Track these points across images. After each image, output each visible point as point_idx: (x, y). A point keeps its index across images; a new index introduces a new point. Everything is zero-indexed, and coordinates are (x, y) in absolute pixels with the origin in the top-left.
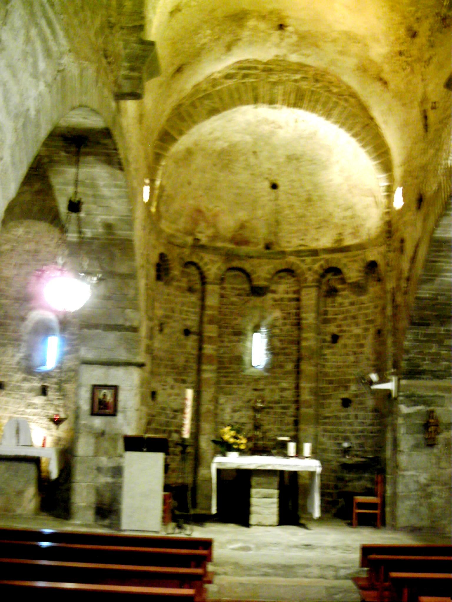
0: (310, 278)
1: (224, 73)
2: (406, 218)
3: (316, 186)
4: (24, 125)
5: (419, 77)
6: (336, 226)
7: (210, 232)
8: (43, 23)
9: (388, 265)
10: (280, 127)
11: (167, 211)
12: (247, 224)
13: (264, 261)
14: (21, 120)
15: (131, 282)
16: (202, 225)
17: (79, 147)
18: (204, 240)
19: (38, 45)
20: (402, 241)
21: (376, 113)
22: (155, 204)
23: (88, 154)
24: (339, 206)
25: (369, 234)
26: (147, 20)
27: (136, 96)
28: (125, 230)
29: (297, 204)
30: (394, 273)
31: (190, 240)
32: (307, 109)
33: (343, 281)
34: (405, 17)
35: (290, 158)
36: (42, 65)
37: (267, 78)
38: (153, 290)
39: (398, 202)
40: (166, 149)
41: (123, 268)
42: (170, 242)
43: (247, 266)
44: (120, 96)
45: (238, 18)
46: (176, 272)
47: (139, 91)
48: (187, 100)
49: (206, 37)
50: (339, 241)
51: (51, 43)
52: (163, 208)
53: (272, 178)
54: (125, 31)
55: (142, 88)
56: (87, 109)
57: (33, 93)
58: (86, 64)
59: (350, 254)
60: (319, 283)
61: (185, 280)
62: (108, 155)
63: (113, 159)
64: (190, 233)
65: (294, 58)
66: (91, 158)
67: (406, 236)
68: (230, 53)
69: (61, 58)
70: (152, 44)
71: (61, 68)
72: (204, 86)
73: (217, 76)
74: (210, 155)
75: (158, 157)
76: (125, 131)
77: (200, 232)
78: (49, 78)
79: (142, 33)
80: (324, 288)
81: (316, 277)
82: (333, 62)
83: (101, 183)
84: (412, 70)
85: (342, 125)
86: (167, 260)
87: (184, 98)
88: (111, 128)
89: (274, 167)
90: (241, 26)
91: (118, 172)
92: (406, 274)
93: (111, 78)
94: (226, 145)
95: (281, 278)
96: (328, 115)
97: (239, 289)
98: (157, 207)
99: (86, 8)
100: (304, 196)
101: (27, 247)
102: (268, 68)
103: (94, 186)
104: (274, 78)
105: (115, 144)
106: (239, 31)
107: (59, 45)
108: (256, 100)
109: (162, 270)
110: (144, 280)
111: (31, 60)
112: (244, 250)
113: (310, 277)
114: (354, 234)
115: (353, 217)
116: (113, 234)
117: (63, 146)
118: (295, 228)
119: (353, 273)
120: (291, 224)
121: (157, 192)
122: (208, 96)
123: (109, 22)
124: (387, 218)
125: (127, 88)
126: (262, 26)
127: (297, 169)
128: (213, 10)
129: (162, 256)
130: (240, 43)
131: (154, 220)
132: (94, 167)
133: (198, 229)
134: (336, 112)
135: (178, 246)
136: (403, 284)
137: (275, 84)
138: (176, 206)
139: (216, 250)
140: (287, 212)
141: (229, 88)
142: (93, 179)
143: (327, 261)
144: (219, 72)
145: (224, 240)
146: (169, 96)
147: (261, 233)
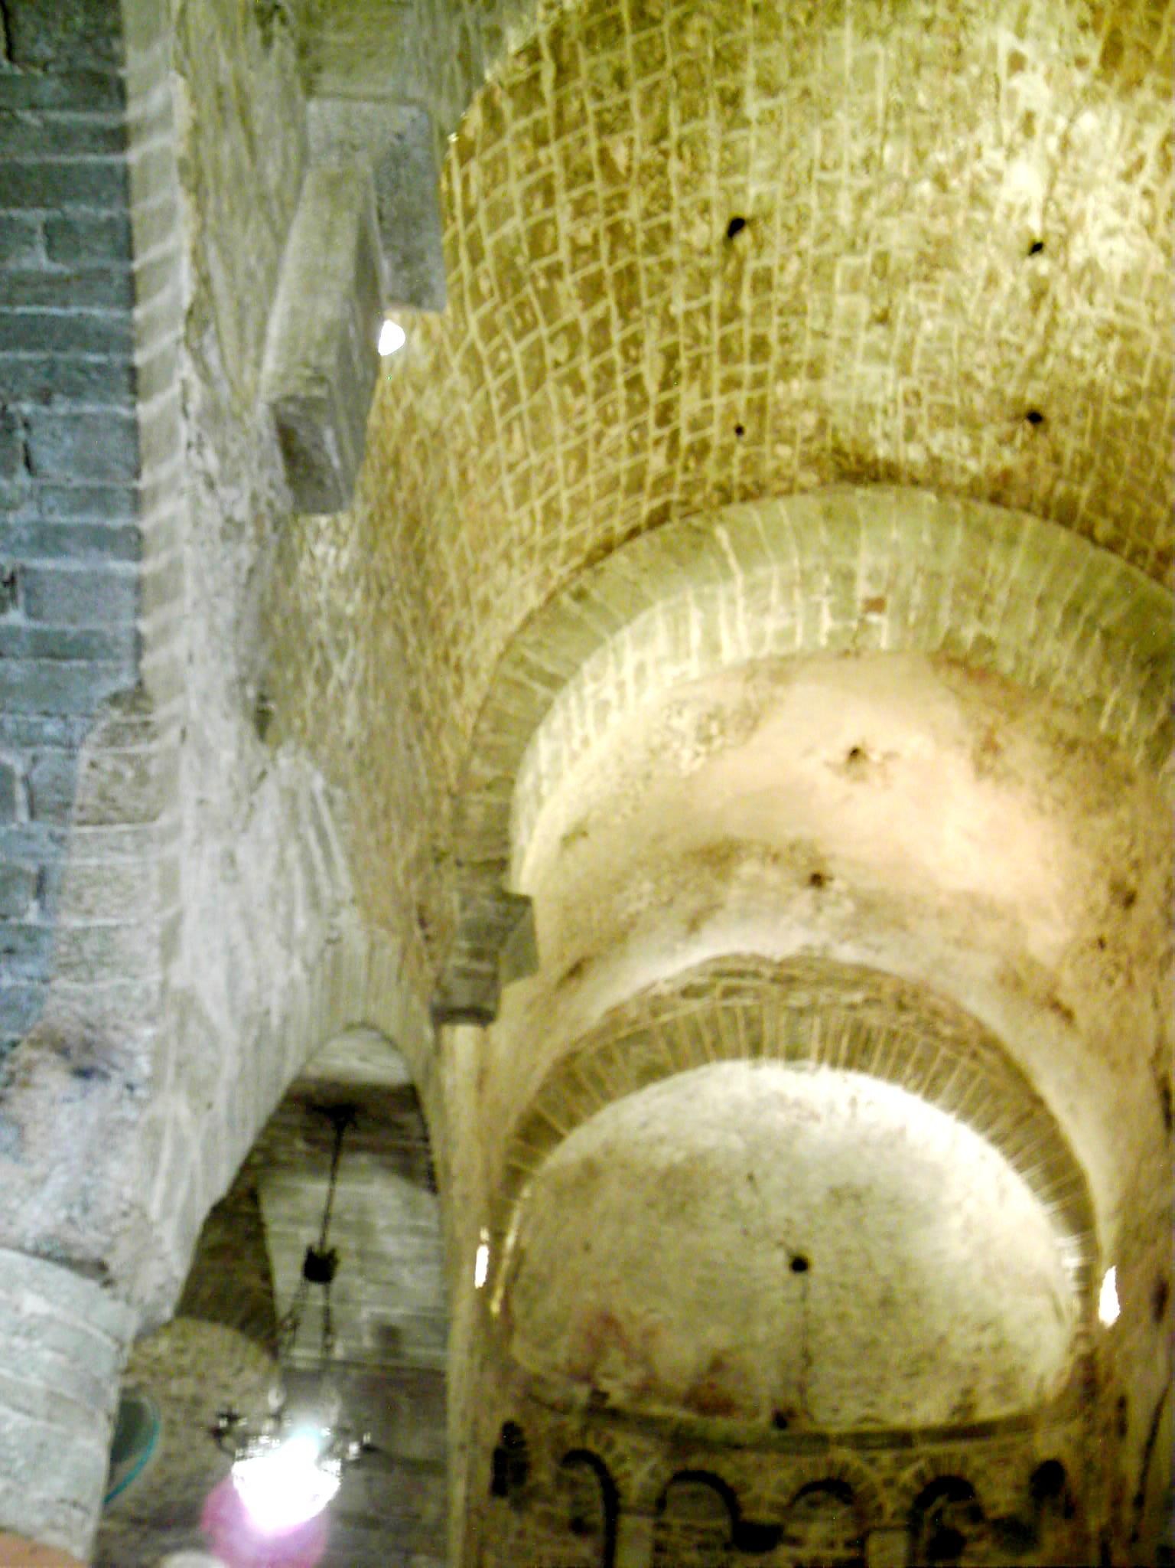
0: (890, 1508)
1: (681, 984)
2: (1128, 1344)
3: (904, 1267)
4: (258, 1044)
5: (1148, 1000)
6: (957, 1368)
7: (635, 1376)
8: (311, 835)
9: (1088, 1466)
10: (815, 1117)
11: (528, 1314)
12: (727, 1360)
13: (773, 1457)
14: (255, 1032)
15: (433, 1484)
16: (615, 1357)
17: (339, 1128)
18: (618, 1396)
19: (299, 880)
20: (1122, 1404)
21: (1048, 1087)
22: (499, 1293)
23: (357, 1148)
24: (964, 1319)
25: (1039, 1392)
26: (516, 849)
27: (481, 1016)
28: (428, 1346)
29: (855, 1313)
30: (1106, 1490)
31: (581, 1394)
32: (878, 1074)
33: (976, 1514)
34: (1106, 860)
35: (838, 1195)
36: (301, 923)
37: (785, 997)
38: (482, 1518)
39: (1109, 1309)
40: (533, 1159)
41: (414, 1446)
42: (532, 1394)
43: (727, 1468)
44: (445, 1015)
45: (718, 857)
46: (543, 1474)
47: (489, 1006)
48: (591, 1044)
49: (640, 898)
50: (965, 1408)
51: (322, 879)
52: (518, 1308)
53: (792, 1243)
54: (465, 871)
55: (497, 999)
56: (374, 1035)
57: (280, 978)
58: (383, 933)
59: (994, 1442)
60: (913, 1523)
61: (564, 1498)
62: (405, 1152)
63: (417, 1165)
64: (587, 1378)
65: (847, 953)
66: (363, 1159)
67: (1131, 1388)
68: (694, 937)
69: (335, 914)
70: (526, 901)
71: (334, 935)
72: (632, 1013)
73: (665, 989)
74: (642, 1179)
75: (514, 1177)
76: (447, 1099)
77: (609, 1376)
78: (311, 953)
79: (503, 877)
80: (927, 1533)
81: (908, 1503)
82: (941, 964)
83: (381, 1222)
84: (1130, 981)
85: (966, 1115)
86: (523, 1443)
87: (581, 1040)
88: (420, 1087)
89: (798, 1217)
90: (724, 876)
91: (425, 1197)
92: (1132, 1488)
93: (430, 973)
94: (679, 1157)
95: (813, 1504)
96: (931, 1091)
97: (702, 1532)
98: (506, 1303)
99: (393, 813)
100: (874, 1292)
101: (175, 1387)
102: (786, 976)
103: (363, 1229)
104: (799, 998)
105: (424, 1125)
106: (718, 887)
107: (334, 884)
108: (756, 1049)
109: (509, 1465)
110: (464, 1483)
111: (282, 909)
112: (721, 1426)
113: (891, 1503)
114: (1005, 1388)
115: (998, 1348)
116: (397, 1355)
117: (303, 1128)
118: (850, 1375)
119: (1001, 1494)
120: (840, 1363)
121: (506, 1264)
122: (641, 1036)
123: (434, 849)
124: (1082, 1348)
125: (462, 998)
126: (773, 876)
127: (857, 1224)
128: (660, 838)
129: (510, 1430)
130: (719, 915)
131: (496, 1334)
132: (369, 1182)
133: (601, 1369)
134: (950, 1083)
135: (552, 1407)
136: (1128, 1514)
137: (801, 1012)
138: (551, 1304)
139: (647, 1425)
140: (831, 1330)
141: (690, 1019)
142: (363, 1210)
143: (934, 1461)
144: (668, 981)
145: (668, 1399)
146: (548, 1032)
147: (765, 1384)
